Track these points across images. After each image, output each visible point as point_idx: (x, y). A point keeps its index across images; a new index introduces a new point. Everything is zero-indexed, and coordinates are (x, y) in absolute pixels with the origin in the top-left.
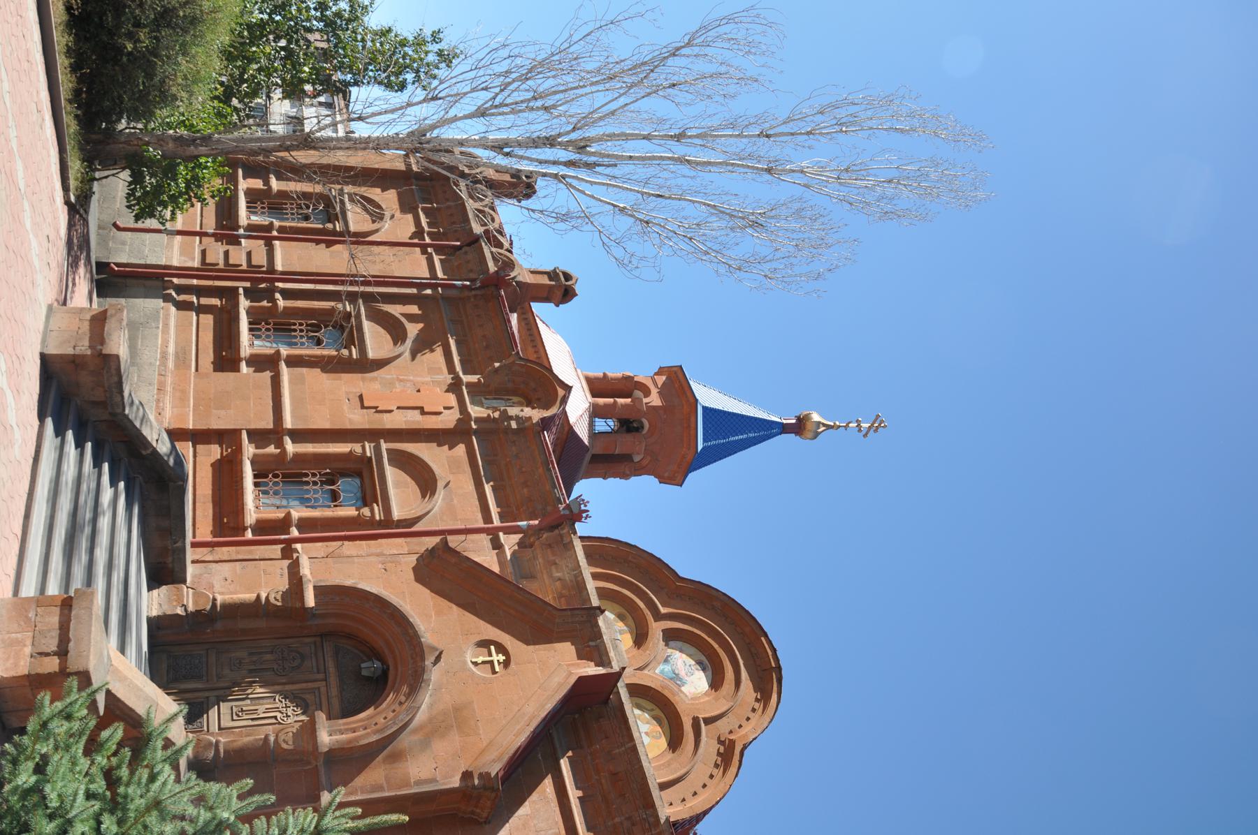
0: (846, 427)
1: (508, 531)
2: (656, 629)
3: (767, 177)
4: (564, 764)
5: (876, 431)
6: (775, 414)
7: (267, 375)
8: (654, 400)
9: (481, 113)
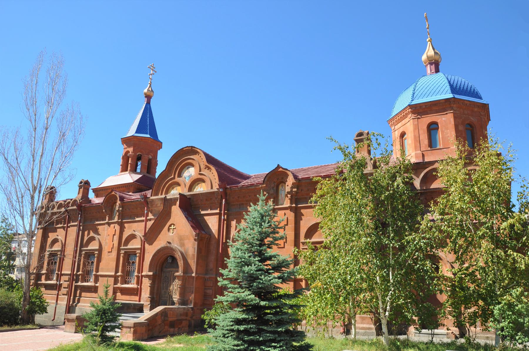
0: (151, 79)
1: (147, 215)
2: (177, 179)
3: (49, 130)
4: (203, 212)
6: (142, 106)
8: (131, 150)
9: (22, 217)
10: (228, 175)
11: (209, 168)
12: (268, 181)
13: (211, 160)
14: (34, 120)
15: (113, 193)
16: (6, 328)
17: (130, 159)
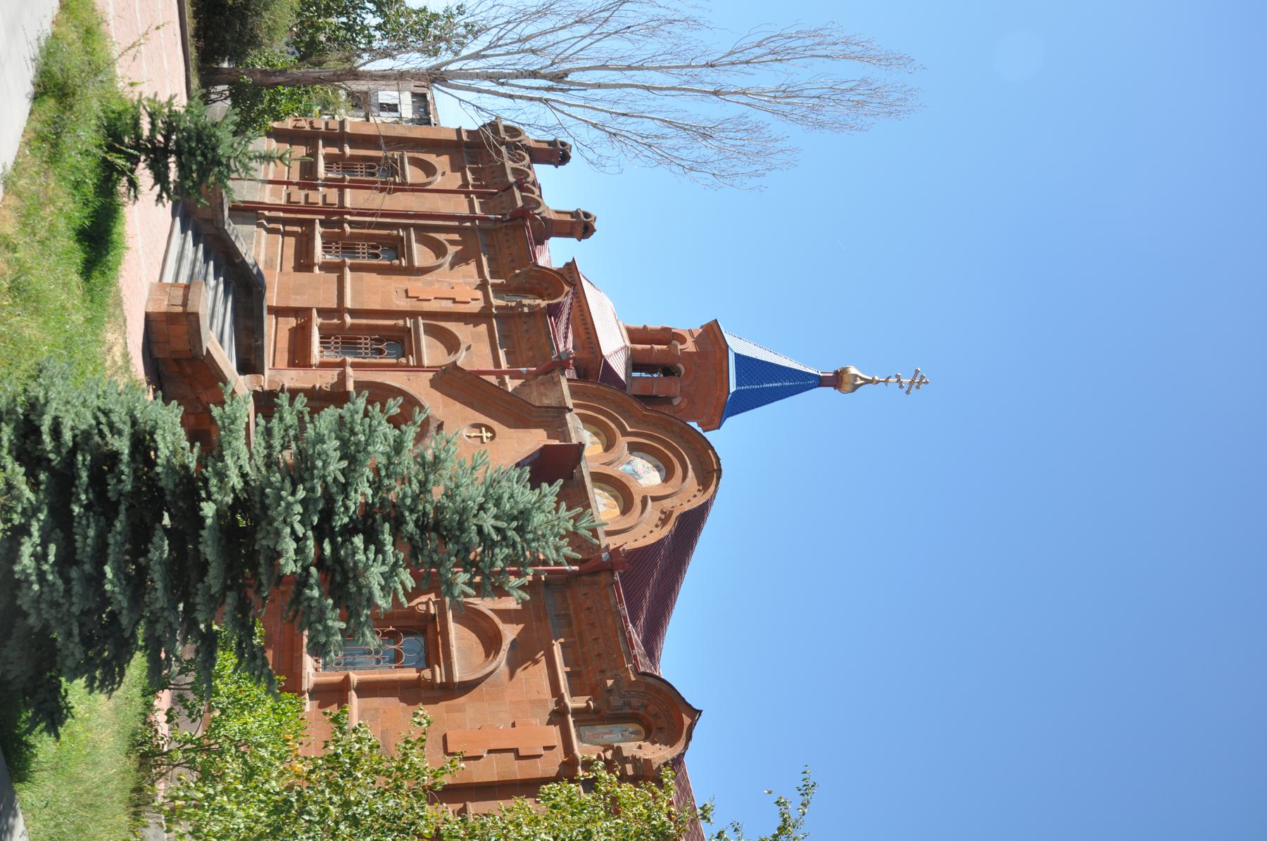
0: (886, 381)
1: (514, 376)
2: (622, 442)
3: (714, 98)
5: (918, 387)
7: (334, 276)
8: (690, 346)
10: (652, 577)
11: (664, 522)
12: (648, 686)
13: (689, 526)
14: (736, 60)
15: (567, 288)
16: (191, 24)
17: (665, 347)
